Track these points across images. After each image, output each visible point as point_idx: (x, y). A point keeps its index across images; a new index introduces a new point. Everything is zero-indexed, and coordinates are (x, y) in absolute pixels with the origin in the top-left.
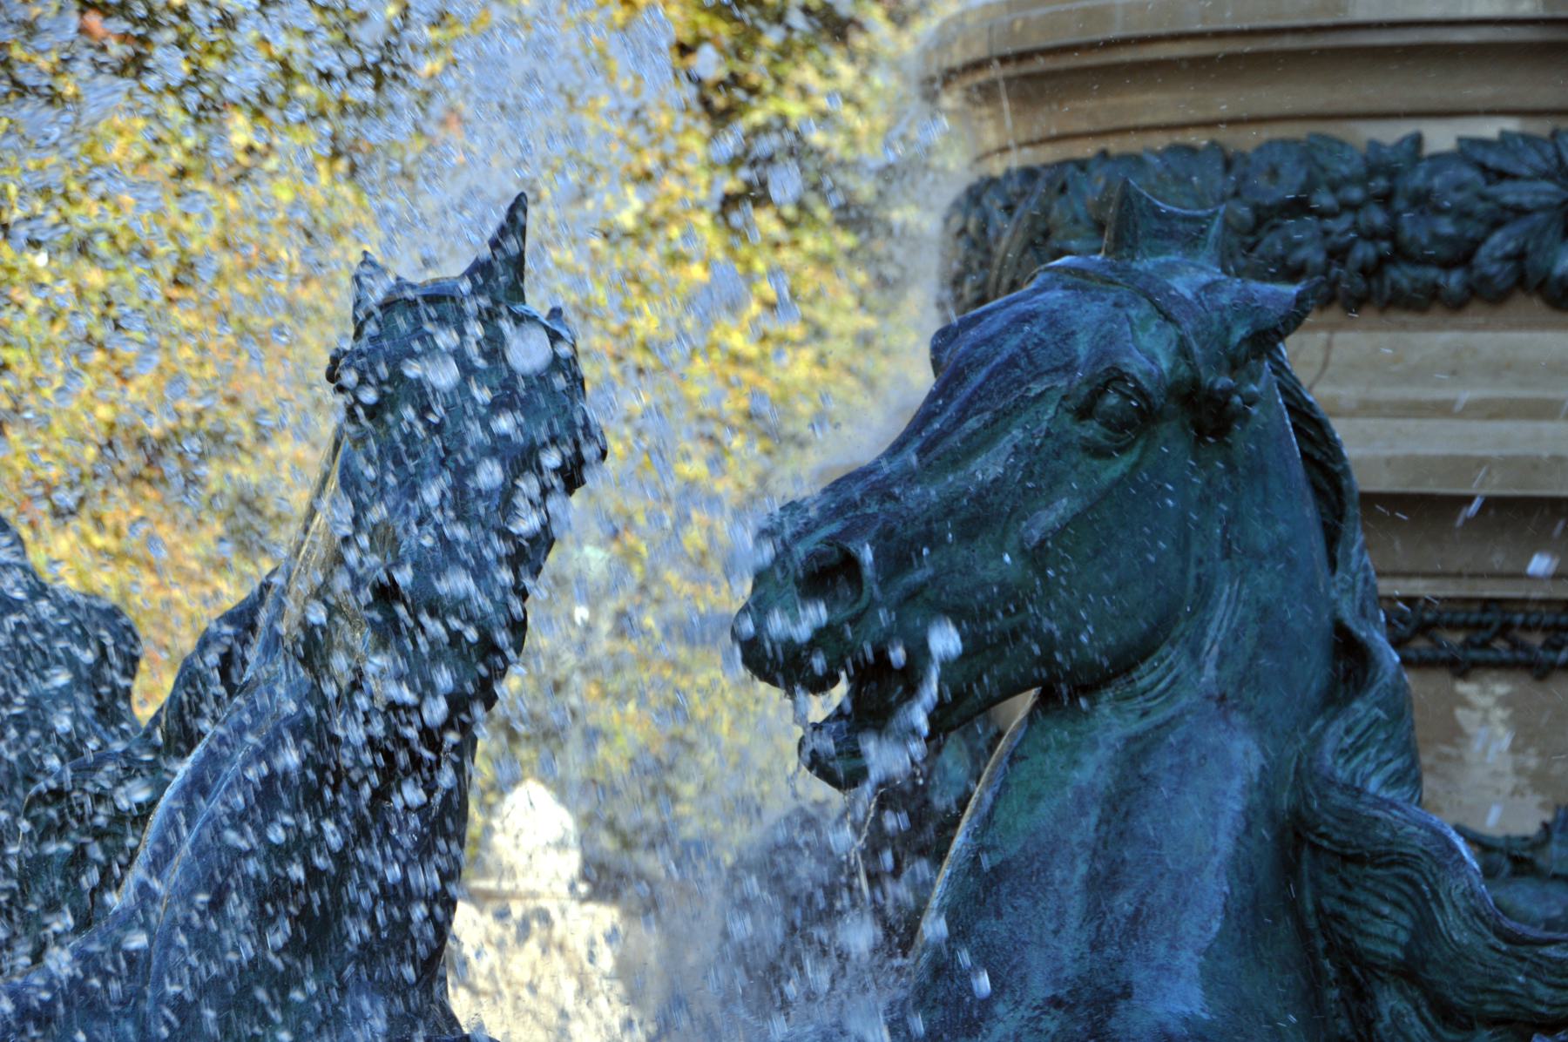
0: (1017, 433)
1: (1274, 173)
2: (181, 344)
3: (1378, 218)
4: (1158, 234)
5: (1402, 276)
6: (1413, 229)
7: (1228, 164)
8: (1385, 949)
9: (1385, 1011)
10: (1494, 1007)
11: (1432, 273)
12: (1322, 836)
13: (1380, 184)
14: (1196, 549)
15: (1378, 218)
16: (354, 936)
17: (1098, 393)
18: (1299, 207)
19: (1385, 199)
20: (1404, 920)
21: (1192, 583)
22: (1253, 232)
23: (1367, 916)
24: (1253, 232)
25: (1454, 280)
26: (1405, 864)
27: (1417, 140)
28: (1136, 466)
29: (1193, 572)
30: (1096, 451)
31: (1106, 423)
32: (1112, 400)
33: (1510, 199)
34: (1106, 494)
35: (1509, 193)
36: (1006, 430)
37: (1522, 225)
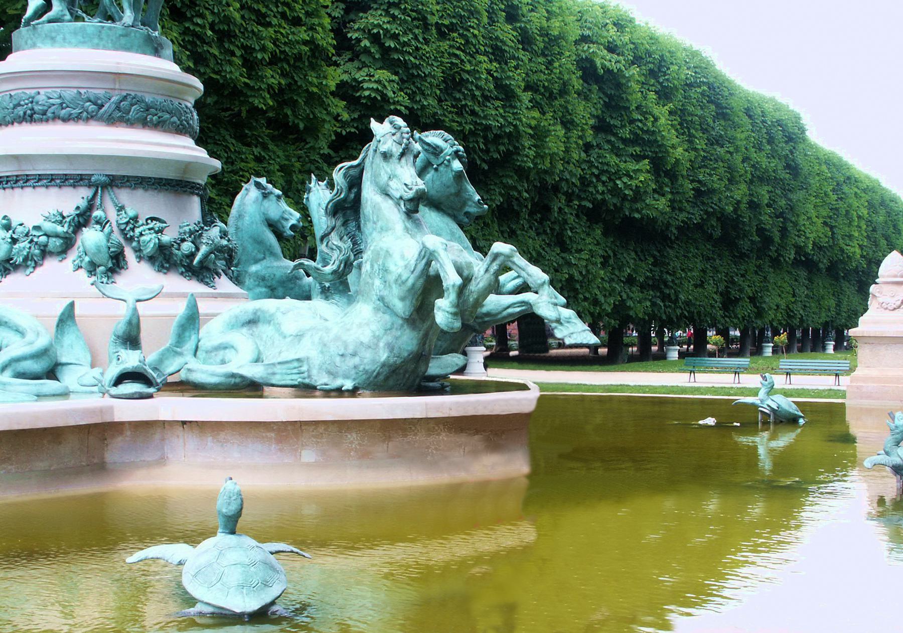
6: (36, 108)
19: (32, 102)
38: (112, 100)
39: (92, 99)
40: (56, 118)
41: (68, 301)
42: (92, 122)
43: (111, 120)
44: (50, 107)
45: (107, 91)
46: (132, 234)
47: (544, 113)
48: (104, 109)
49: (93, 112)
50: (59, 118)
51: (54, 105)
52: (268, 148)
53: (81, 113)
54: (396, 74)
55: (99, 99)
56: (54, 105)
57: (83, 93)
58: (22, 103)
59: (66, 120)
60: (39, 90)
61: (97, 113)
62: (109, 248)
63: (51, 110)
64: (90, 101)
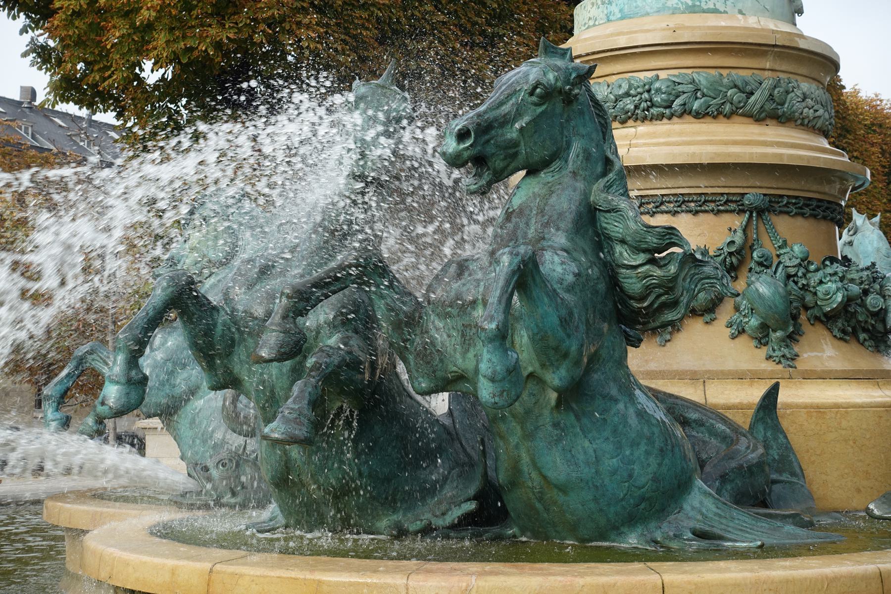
0: (514, 100)
1: (620, 86)
2: (361, 114)
3: (646, 95)
4: (553, 52)
5: (654, 111)
6: (657, 99)
7: (608, 86)
8: (617, 235)
9: (618, 251)
10: (644, 246)
11: (662, 110)
12: (600, 206)
13: (647, 87)
14: (565, 133)
15: (646, 95)
16: (158, 75)
17: (535, 88)
18: (627, 94)
19: (649, 91)
20: (621, 226)
21: (564, 143)
22: (615, 102)
23: (612, 226)
24: (615, 102)
25: (667, 111)
26: (620, 211)
27: (658, 76)
28: (546, 108)
29: (565, 139)
30: (536, 105)
31: (537, 97)
32: (538, 90)
33: (681, 90)
34: (538, 116)
35: (680, 88)
36: (511, 99)
37: (685, 95)
38: (764, 85)
39: (739, 83)
40: (686, 112)
41: (774, 381)
42: (736, 118)
43: (760, 117)
44: (677, 97)
45: (755, 72)
46: (804, 282)
47: (192, 524)
48: (753, 98)
49: (740, 102)
50: (690, 113)
51: (684, 93)
52: (467, 351)
53: (723, 104)
54: (277, 378)
55: (747, 83)
56: (684, 93)
57: (725, 75)
58: (632, 92)
59: (698, 115)
60: (659, 73)
61: (745, 103)
62: (791, 303)
63: (678, 102)
64: (736, 86)
